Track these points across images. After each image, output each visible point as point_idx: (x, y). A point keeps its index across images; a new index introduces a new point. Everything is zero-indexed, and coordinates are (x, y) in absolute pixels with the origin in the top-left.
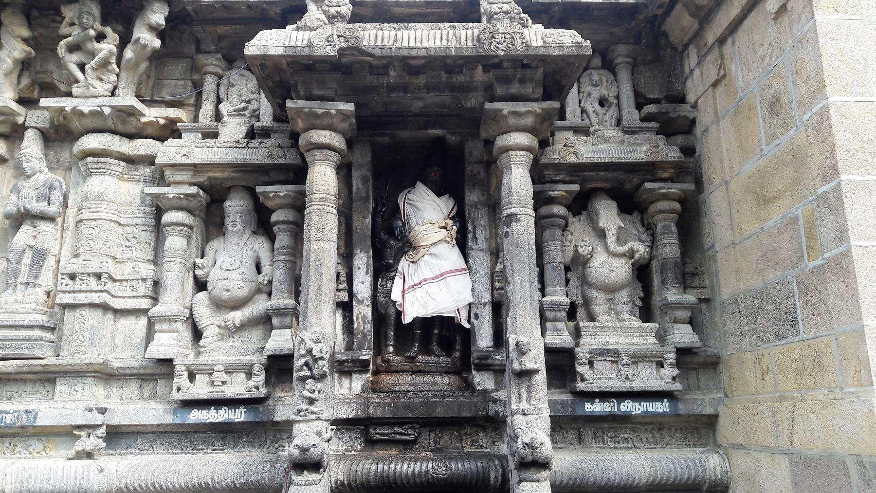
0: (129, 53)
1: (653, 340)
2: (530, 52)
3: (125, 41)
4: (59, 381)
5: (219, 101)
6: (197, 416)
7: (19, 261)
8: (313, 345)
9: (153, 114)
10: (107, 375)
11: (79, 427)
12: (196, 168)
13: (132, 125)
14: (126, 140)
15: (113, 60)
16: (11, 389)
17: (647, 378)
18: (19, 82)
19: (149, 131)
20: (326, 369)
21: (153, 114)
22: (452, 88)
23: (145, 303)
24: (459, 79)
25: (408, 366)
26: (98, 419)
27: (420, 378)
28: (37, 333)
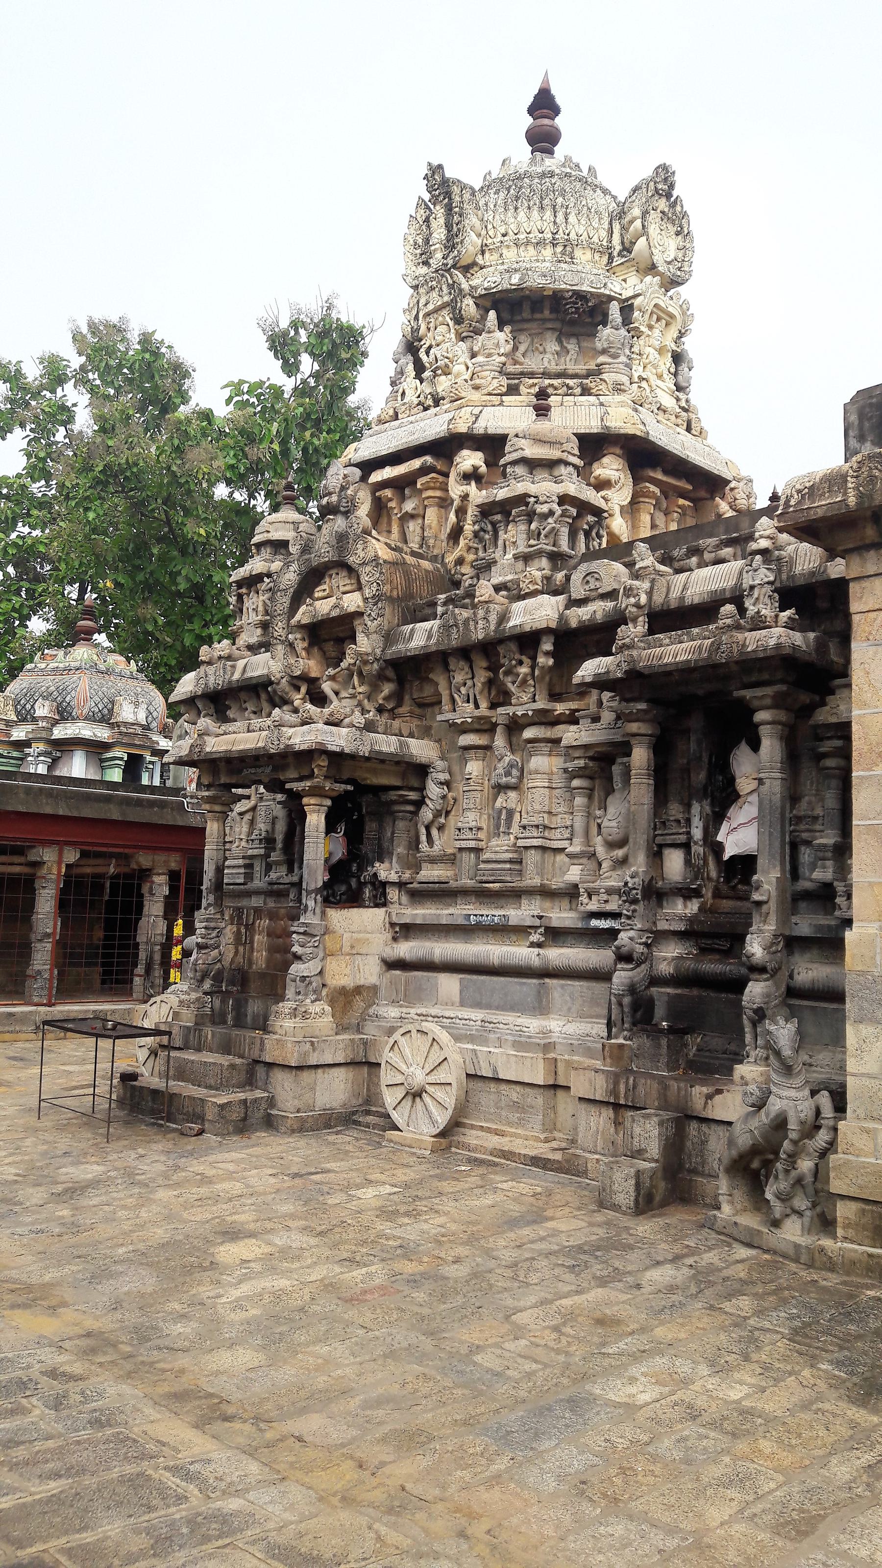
4: (523, 897)
6: (595, 923)
7: (499, 818)
8: (629, 879)
9: (560, 708)
10: (546, 893)
11: (530, 927)
12: (586, 747)
14: (549, 728)
16: (502, 902)
18: (490, 694)
20: (639, 896)
21: (560, 708)
25: (731, 893)
26: (537, 922)
28: (508, 866)
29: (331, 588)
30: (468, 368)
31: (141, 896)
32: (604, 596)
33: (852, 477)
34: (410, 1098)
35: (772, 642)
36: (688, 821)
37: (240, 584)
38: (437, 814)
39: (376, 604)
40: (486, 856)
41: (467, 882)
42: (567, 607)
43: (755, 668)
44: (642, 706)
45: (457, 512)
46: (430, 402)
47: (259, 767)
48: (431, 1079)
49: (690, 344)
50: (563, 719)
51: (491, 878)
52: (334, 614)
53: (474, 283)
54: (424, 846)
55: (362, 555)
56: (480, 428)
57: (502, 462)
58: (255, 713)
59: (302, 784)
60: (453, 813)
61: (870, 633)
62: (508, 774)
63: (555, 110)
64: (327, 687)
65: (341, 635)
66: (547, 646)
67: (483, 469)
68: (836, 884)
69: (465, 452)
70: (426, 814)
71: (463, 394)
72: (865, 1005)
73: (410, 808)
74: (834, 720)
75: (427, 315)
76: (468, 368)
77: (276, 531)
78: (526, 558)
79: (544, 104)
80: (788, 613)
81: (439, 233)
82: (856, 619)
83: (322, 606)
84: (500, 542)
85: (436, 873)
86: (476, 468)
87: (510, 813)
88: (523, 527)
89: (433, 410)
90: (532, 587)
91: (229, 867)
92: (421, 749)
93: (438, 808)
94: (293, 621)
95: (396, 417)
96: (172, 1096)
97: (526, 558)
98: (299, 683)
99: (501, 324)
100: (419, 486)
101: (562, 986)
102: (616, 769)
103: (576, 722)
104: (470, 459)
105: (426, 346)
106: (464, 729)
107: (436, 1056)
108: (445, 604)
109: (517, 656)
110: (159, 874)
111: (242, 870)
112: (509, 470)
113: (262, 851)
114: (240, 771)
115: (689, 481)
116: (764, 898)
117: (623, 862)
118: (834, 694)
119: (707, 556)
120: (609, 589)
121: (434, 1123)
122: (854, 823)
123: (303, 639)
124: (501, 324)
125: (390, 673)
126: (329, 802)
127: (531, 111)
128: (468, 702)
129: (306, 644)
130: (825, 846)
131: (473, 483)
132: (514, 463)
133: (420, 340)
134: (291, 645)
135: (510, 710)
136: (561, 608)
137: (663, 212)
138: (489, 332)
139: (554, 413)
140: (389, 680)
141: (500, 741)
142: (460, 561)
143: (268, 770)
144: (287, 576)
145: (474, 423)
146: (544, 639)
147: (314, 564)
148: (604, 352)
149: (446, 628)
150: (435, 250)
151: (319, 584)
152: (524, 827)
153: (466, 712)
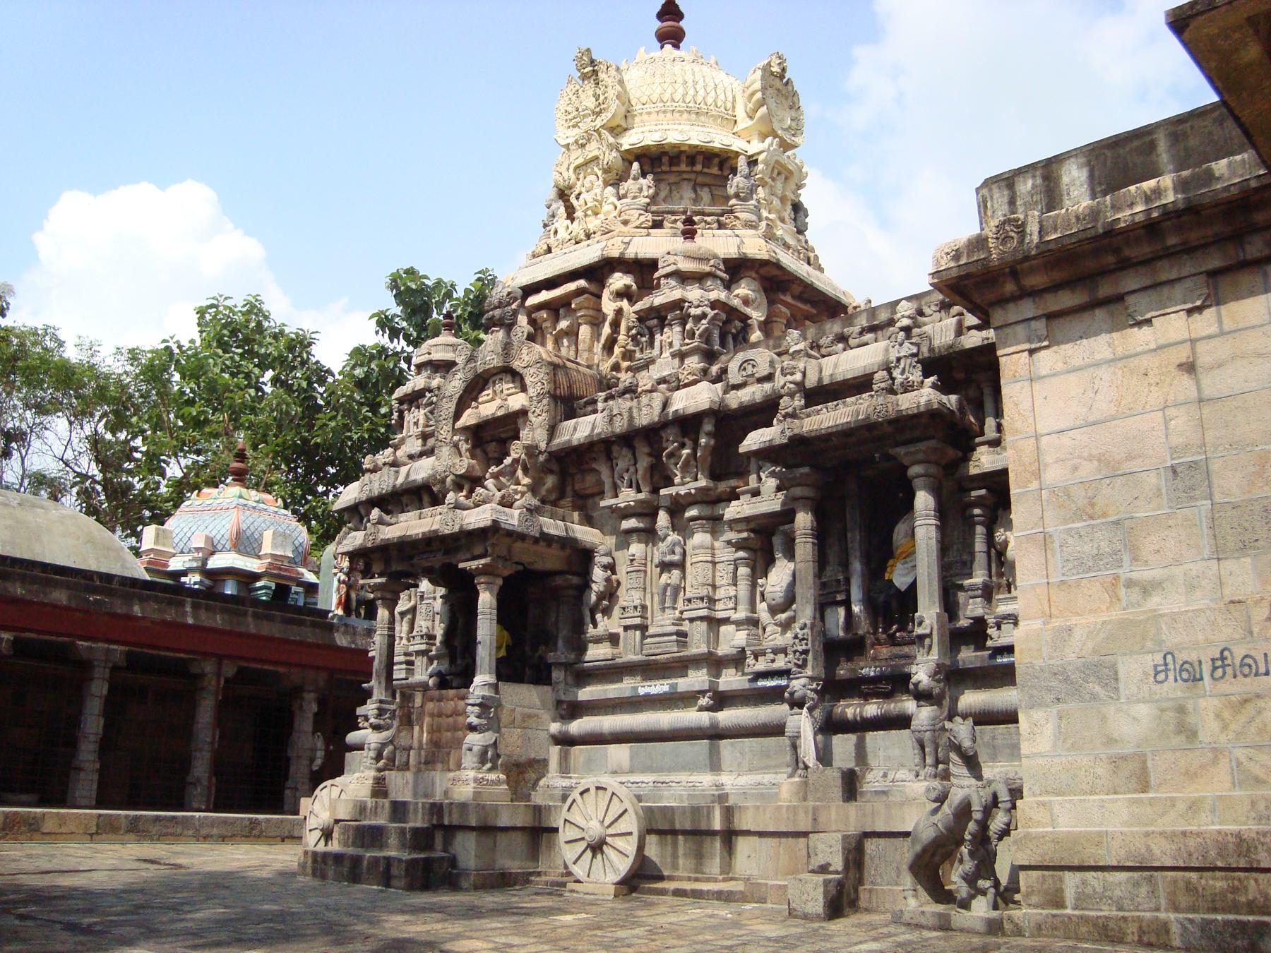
6: (761, 683)
32: (760, 380)
35: (923, 400)
36: (848, 581)
37: (401, 401)
39: (540, 401)
40: (651, 631)
41: (632, 657)
42: (725, 392)
44: (806, 470)
45: (611, 325)
46: (582, 237)
48: (610, 831)
49: (805, 198)
50: (724, 497)
51: (659, 651)
52: (500, 413)
55: (526, 358)
56: (630, 253)
57: (656, 275)
59: (476, 562)
63: (679, 16)
65: (503, 436)
66: (708, 427)
67: (634, 287)
69: (617, 275)
72: (1035, 692)
78: (681, 356)
80: (932, 379)
82: (1002, 360)
83: (487, 407)
84: (657, 344)
86: (628, 287)
88: (677, 329)
92: (585, 534)
94: (459, 424)
95: (549, 250)
96: (362, 847)
97: (681, 356)
98: (464, 482)
101: (732, 745)
102: (777, 541)
104: (619, 280)
106: (626, 513)
107: (616, 809)
108: (606, 400)
109: (680, 439)
110: (310, 691)
111: (404, 666)
112: (663, 281)
114: (411, 558)
115: (813, 306)
116: (927, 631)
117: (786, 626)
119: (852, 342)
120: (766, 373)
121: (615, 870)
123: (466, 441)
125: (555, 467)
132: (667, 276)
134: (456, 446)
135: (672, 491)
136: (720, 393)
137: (778, 90)
139: (697, 238)
140: (551, 472)
141: (663, 519)
142: (616, 367)
143: (439, 556)
144: (453, 384)
146: (706, 420)
147: (479, 371)
149: (611, 419)
151: (483, 390)
152: (689, 601)
153: (627, 497)
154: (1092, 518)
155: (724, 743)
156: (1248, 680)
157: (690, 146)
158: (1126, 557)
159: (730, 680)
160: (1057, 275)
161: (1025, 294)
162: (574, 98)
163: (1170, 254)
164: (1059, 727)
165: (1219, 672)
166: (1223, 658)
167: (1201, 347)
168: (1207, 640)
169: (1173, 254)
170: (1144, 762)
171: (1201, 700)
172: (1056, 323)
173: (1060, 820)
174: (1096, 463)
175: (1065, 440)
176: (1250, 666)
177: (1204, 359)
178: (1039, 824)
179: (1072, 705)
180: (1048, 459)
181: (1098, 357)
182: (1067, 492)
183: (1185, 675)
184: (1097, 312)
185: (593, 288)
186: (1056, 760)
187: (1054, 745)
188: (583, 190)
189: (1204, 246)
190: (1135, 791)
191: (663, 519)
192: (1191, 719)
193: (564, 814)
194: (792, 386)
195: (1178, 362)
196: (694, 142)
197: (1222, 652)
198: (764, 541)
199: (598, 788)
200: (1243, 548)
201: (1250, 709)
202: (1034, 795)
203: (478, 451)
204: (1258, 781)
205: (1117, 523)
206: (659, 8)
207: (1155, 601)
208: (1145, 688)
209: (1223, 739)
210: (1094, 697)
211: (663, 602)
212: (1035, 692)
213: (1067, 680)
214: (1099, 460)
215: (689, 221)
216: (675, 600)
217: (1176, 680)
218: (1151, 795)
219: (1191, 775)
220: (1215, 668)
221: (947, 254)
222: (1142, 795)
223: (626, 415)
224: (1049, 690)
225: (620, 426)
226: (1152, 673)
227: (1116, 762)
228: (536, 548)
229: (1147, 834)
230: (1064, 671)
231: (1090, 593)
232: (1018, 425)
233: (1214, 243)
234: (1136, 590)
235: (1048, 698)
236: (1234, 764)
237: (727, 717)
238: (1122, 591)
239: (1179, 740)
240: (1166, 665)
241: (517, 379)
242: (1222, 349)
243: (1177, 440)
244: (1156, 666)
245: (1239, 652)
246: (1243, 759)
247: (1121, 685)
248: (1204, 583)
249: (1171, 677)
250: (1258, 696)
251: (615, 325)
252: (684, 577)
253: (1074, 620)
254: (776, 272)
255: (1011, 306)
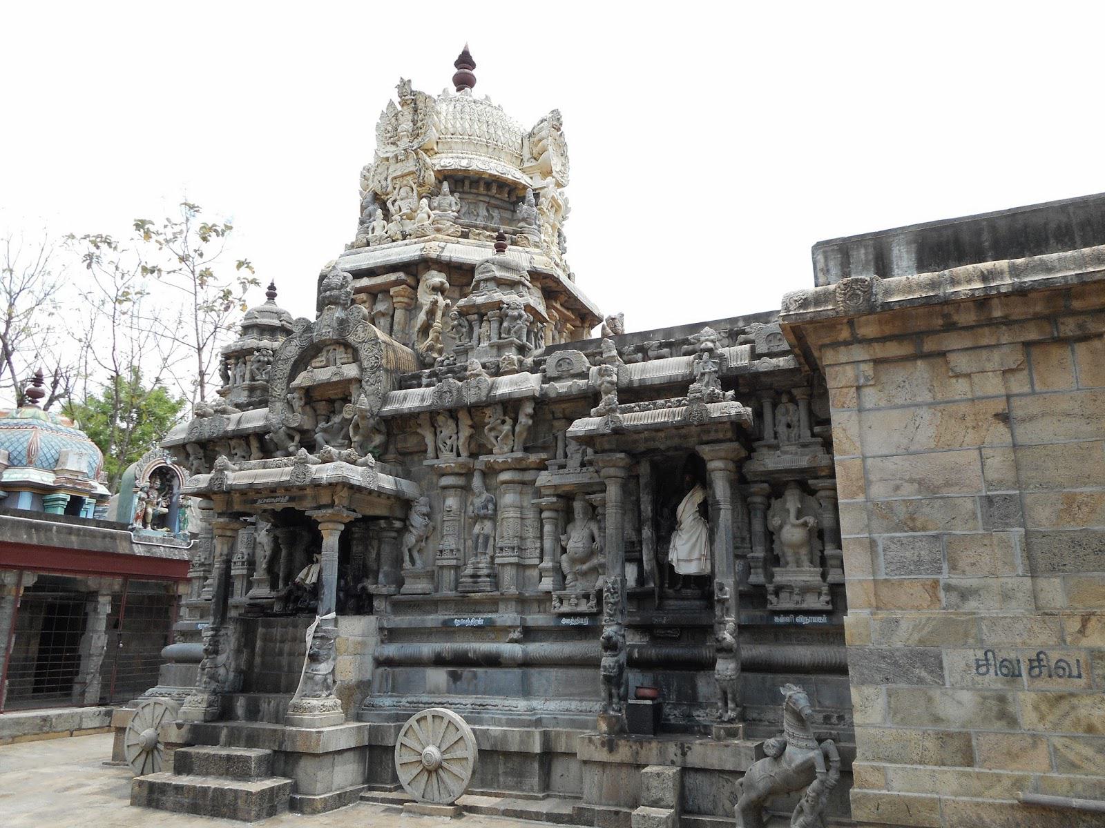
0: (517, 429)
1: (820, 579)
2: (818, 362)
3: (515, 421)
5: (566, 446)
6: (565, 621)
9: (533, 458)
11: (509, 627)
13: (524, 465)
15: (511, 433)
17: (812, 602)
19: (533, 466)
22: (680, 436)
23: (536, 561)
24: (683, 431)
27: (681, 603)
29: (328, 360)
30: (429, 217)
31: (86, 614)
33: (840, 293)
34: (426, 775)
38: (419, 540)
43: (708, 429)
45: (427, 313)
46: (399, 236)
47: (275, 498)
48: (447, 756)
49: (565, 231)
52: (335, 379)
53: (434, 162)
54: (407, 564)
55: (362, 335)
58: (244, 457)
60: (432, 538)
61: (844, 403)
62: (486, 507)
63: (472, 65)
64: (319, 437)
67: (447, 285)
68: (767, 585)
70: (410, 539)
71: (428, 233)
72: (866, 671)
73: (394, 534)
74: (762, 469)
75: (395, 178)
76: (429, 217)
77: (263, 318)
79: (465, 61)
81: (406, 126)
83: (320, 373)
85: (420, 586)
86: (442, 283)
87: (487, 538)
89: (400, 242)
90: (511, 368)
91: (498, 557)
93: (422, 534)
95: (368, 244)
99: (452, 192)
100: (391, 294)
103: (546, 469)
105: (392, 199)
108: (429, 376)
109: (502, 418)
113: (245, 572)
118: (755, 451)
122: (842, 537)
124: (452, 192)
125: (383, 428)
126: (342, 527)
127: (457, 64)
128: (452, 451)
129: (302, 403)
130: (758, 558)
131: (439, 293)
132: (487, 280)
133: (387, 194)
138: (445, 195)
140: (379, 432)
141: (477, 482)
145: (442, 252)
148: (524, 220)
150: (403, 136)
154: (913, 529)
155: (534, 671)
156: (1060, 680)
157: (490, 175)
158: (945, 566)
159: (537, 619)
160: (888, 330)
161: (856, 340)
162: (393, 120)
163: (991, 323)
164: (889, 702)
165: (1036, 671)
166: (1039, 660)
167: (1016, 402)
168: (1024, 643)
169: (994, 324)
170: (970, 741)
171: (1020, 693)
172: (881, 367)
173: (894, 784)
174: (916, 485)
175: (889, 464)
176: (1064, 669)
177: (1018, 413)
178: (873, 786)
179: (902, 685)
180: (872, 477)
181: (919, 399)
182: (889, 506)
183: (1005, 671)
184: (919, 362)
185: (410, 280)
186: (887, 732)
187: (885, 720)
188: (398, 198)
189: (1022, 322)
190: (961, 765)
191: (477, 482)
192: (1011, 709)
193: (401, 738)
194: (609, 385)
195: (996, 411)
196: (493, 172)
197: (1038, 655)
198: (565, 506)
199: (434, 716)
200: (1053, 570)
201: (1065, 706)
202: (867, 759)
203: (308, 408)
204: (1074, 766)
205: (936, 537)
206: (457, 58)
207: (972, 604)
208: (968, 677)
209: (1040, 727)
210: (921, 681)
211: (476, 548)
212: (866, 671)
213: (895, 664)
214: (919, 483)
215: (501, 237)
216: (486, 546)
217: (997, 675)
218: (977, 770)
219: (1012, 756)
220: (1032, 668)
221: (796, 301)
222: (968, 769)
223: (455, 393)
224: (879, 670)
225: (448, 401)
226: (974, 666)
227: (944, 738)
228: (369, 497)
229: (978, 804)
230: (892, 656)
231: (912, 591)
232: (847, 447)
233: (1031, 319)
234: (954, 594)
235: (878, 677)
236: (1051, 749)
237: (537, 649)
238: (942, 594)
239: (1000, 725)
240: (987, 660)
241: (350, 351)
242: (1034, 406)
243: (992, 475)
244: (977, 660)
245: (1054, 656)
246: (1059, 747)
247: (946, 673)
248: (1020, 595)
249: (992, 671)
250: (1072, 695)
251: (431, 313)
252: (495, 529)
253: (899, 614)
254: (554, 285)
255: (842, 349)
